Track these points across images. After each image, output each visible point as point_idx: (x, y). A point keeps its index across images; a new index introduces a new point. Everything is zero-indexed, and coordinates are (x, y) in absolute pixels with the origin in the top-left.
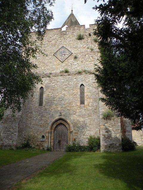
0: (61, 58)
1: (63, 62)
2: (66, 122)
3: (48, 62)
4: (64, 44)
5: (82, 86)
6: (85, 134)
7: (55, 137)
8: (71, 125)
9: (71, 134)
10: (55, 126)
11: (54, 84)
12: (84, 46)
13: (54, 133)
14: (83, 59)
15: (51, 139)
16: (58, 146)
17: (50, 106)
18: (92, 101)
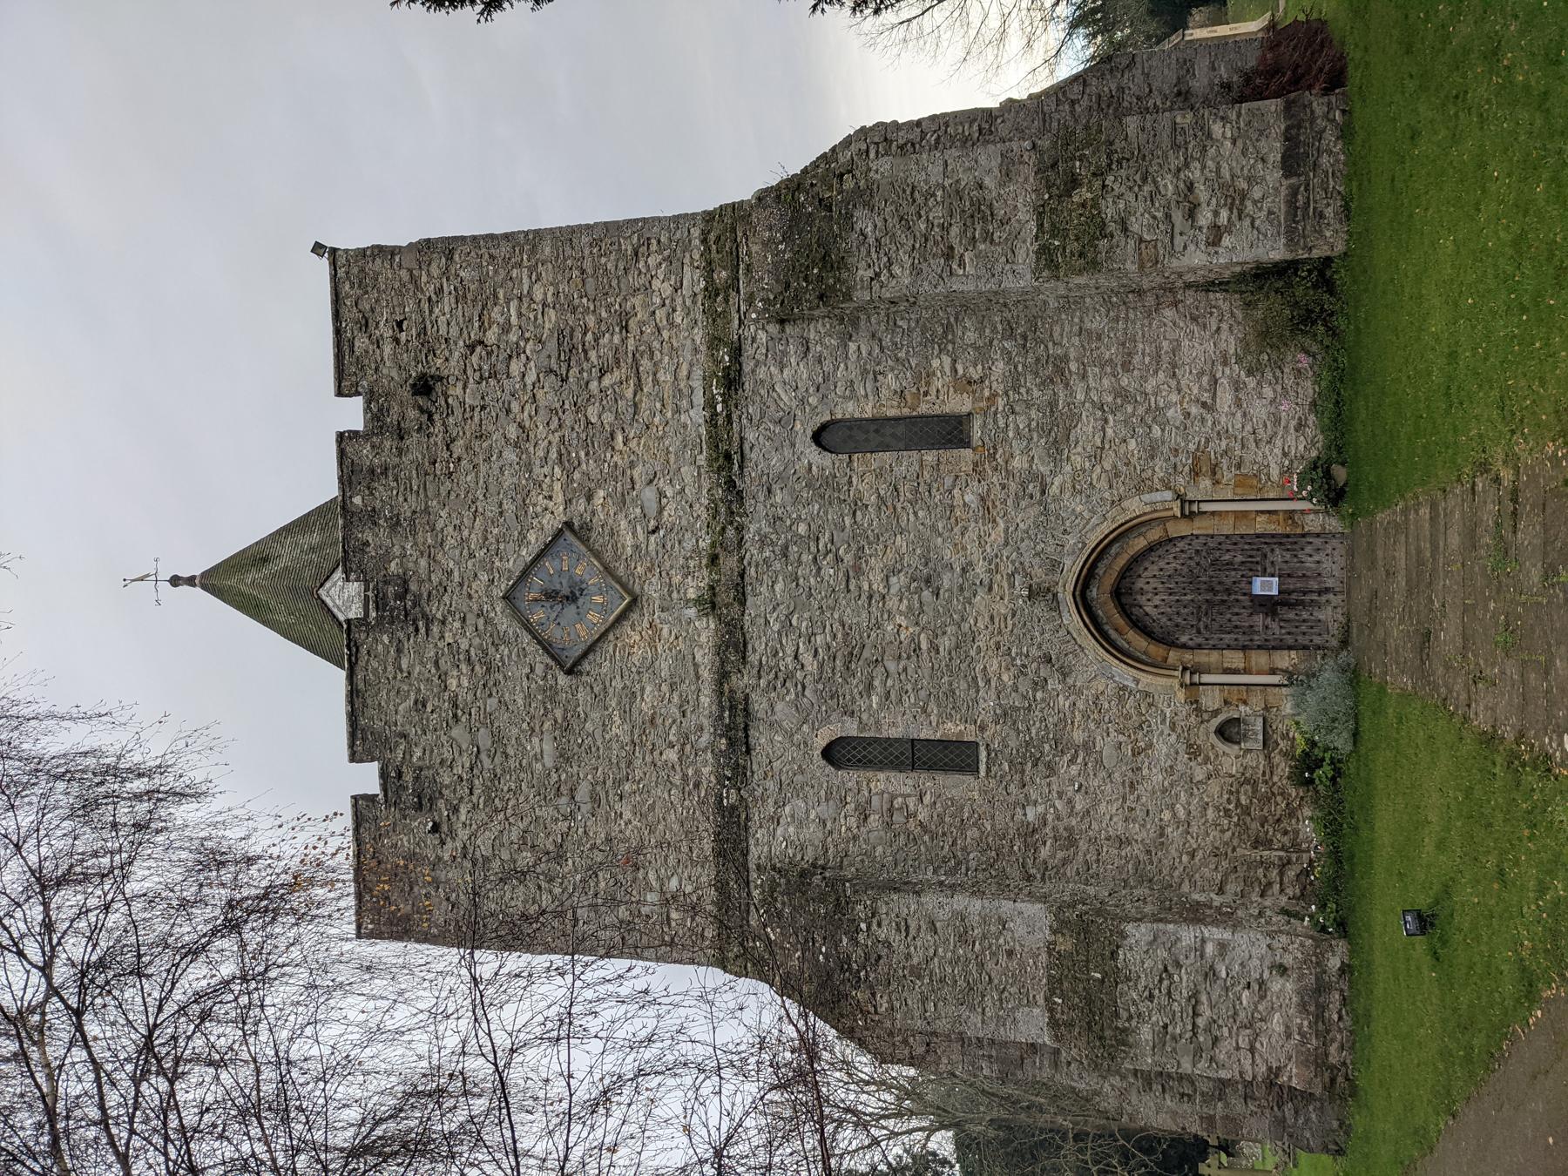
0: (604, 609)
1: (629, 592)
2: (1123, 534)
3: (626, 713)
4: (486, 591)
5: (826, 438)
6: (1206, 397)
7: (1228, 638)
8: (1135, 506)
9: (1205, 507)
10: (1138, 642)
11: (807, 658)
12: (513, 432)
13: (1199, 647)
14: (620, 438)
15: (1247, 671)
16: (1305, 615)
17: (975, 679)
18: (947, 361)
